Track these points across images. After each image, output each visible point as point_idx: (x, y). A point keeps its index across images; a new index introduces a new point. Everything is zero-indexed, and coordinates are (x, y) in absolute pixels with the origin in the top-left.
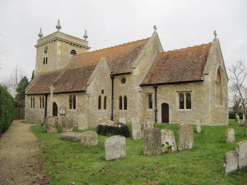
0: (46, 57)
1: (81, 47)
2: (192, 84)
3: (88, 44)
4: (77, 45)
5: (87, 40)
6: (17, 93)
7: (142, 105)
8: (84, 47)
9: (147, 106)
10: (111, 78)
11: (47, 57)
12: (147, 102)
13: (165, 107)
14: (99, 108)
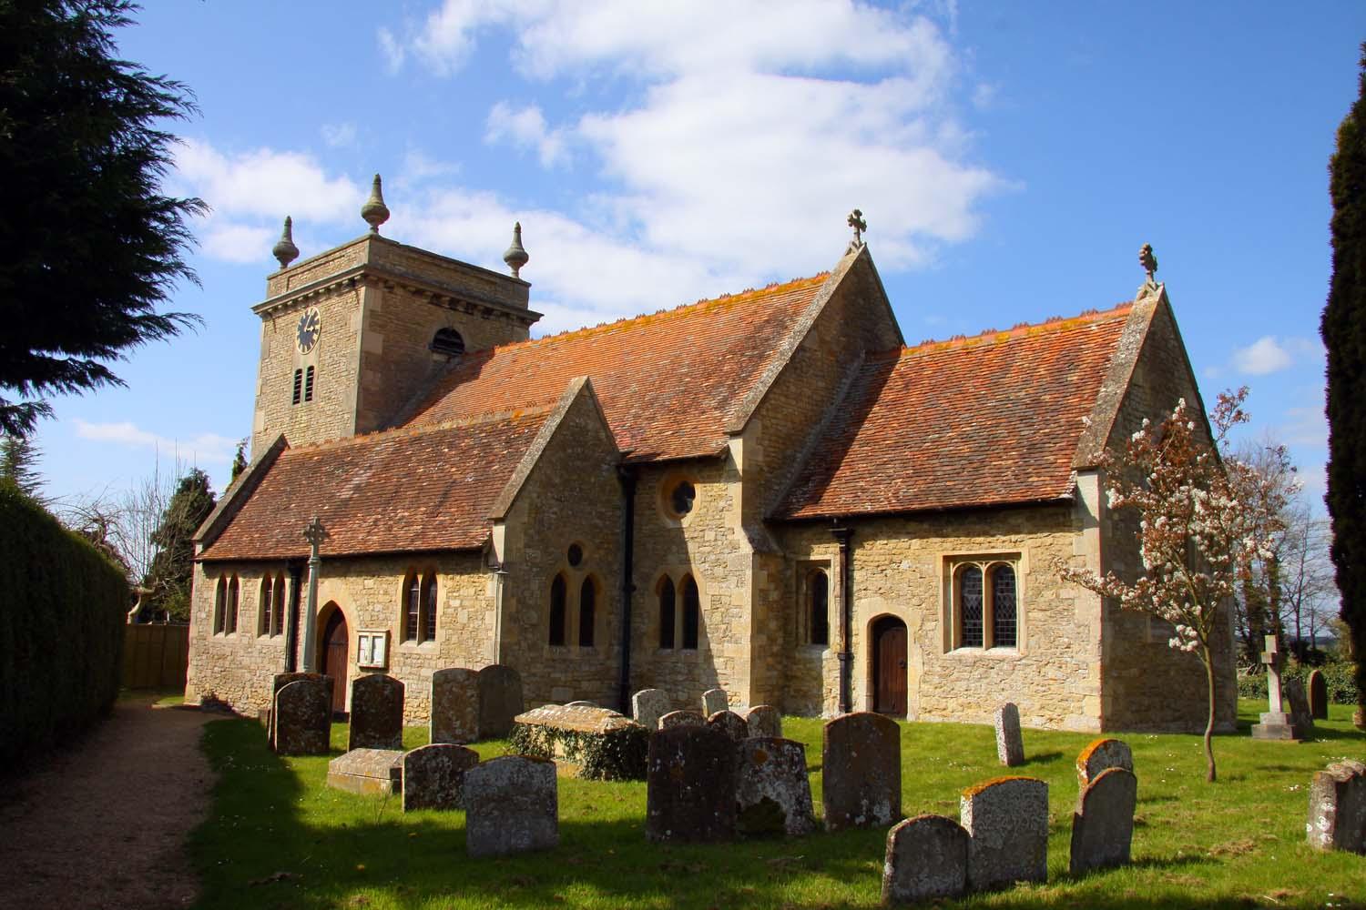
0: (309, 365)
2: (1020, 521)
3: (526, 298)
4: (468, 304)
5: (525, 273)
6: (153, 548)
7: (773, 625)
8: (506, 310)
9: (801, 630)
10: (622, 479)
11: (311, 368)
12: (802, 609)
13: (888, 631)
14: (557, 637)
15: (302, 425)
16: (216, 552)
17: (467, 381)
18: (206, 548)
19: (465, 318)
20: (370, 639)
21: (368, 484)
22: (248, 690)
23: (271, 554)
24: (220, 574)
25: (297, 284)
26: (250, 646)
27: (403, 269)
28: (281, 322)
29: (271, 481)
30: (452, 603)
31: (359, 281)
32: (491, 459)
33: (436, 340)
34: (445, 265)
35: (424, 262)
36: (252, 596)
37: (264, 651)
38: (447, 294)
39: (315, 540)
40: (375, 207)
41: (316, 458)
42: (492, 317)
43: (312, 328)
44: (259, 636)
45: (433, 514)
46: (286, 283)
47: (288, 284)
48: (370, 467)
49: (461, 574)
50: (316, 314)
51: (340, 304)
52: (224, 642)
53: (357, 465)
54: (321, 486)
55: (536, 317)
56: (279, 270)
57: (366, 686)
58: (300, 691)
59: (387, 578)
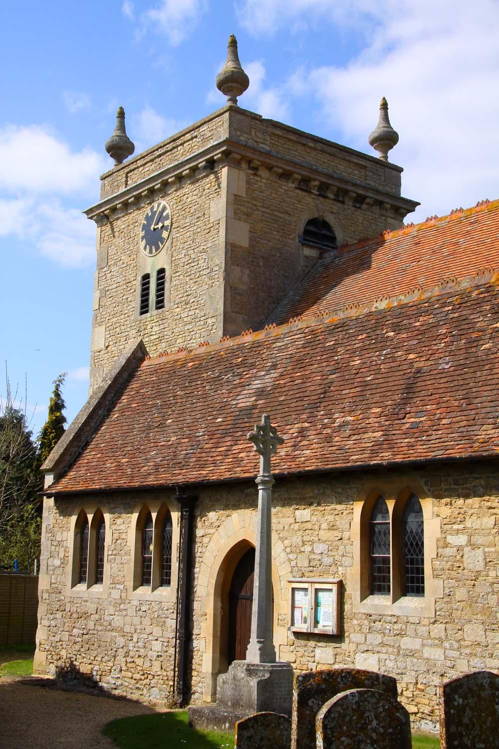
1: (360, 200)
4: (339, 189)
5: (394, 157)
8: (380, 198)
11: (162, 271)
15: (152, 338)
16: (71, 482)
17: (354, 273)
18: (58, 479)
19: (337, 207)
20: (311, 594)
21: (276, 387)
22: (121, 660)
23: (151, 481)
24: (77, 511)
25: (136, 179)
26: (122, 601)
27: (267, 148)
28: (120, 224)
29: (133, 397)
30: (450, 539)
31: (220, 161)
32: (474, 336)
33: (306, 232)
34: (311, 145)
35: (290, 140)
36: (123, 536)
37: (143, 609)
38: (318, 177)
39: (265, 448)
40: (233, 72)
41: (190, 364)
42: (364, 206)
43: (160, 225)
44: (135, 588)
45: (397, 414)
46: (124, 179)
47: (127, 181)
48: (274, 366)
49: (466, 496)
50: (164, 208)
51: (195, 193)
52: (86, 596)
53: (253, 366)
54: (205, 396)
55: (411, 206)
56: (113, 167)
57: (465, 697)
58: (359, 710)
59: (333, 506)
